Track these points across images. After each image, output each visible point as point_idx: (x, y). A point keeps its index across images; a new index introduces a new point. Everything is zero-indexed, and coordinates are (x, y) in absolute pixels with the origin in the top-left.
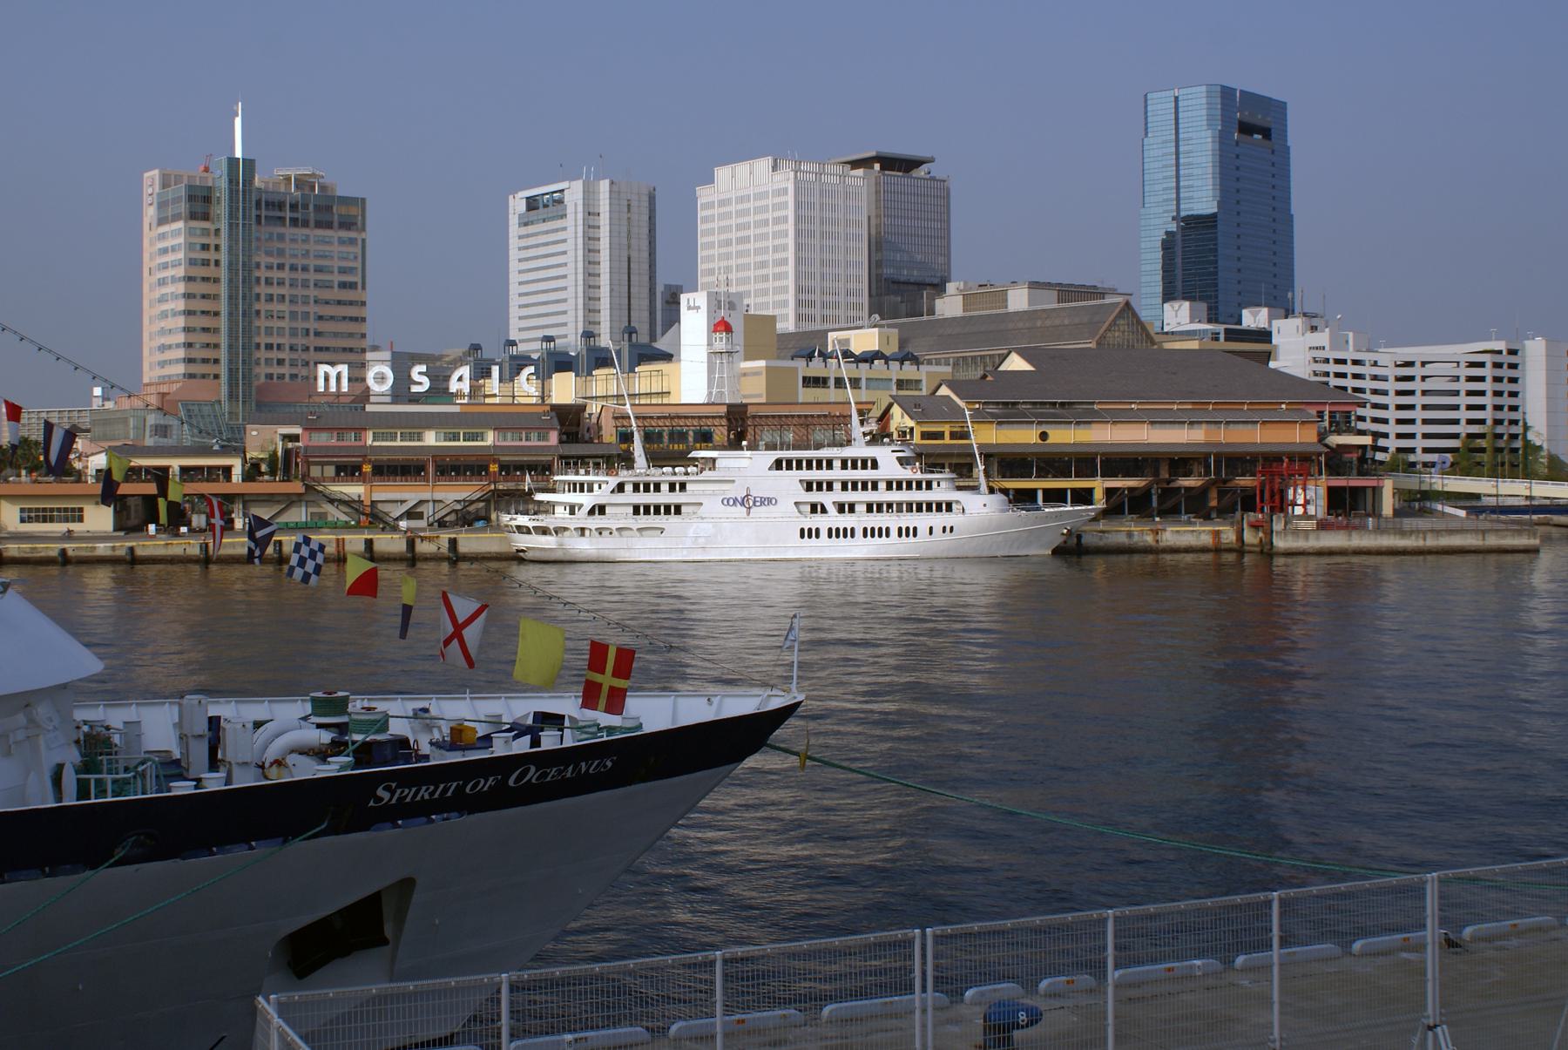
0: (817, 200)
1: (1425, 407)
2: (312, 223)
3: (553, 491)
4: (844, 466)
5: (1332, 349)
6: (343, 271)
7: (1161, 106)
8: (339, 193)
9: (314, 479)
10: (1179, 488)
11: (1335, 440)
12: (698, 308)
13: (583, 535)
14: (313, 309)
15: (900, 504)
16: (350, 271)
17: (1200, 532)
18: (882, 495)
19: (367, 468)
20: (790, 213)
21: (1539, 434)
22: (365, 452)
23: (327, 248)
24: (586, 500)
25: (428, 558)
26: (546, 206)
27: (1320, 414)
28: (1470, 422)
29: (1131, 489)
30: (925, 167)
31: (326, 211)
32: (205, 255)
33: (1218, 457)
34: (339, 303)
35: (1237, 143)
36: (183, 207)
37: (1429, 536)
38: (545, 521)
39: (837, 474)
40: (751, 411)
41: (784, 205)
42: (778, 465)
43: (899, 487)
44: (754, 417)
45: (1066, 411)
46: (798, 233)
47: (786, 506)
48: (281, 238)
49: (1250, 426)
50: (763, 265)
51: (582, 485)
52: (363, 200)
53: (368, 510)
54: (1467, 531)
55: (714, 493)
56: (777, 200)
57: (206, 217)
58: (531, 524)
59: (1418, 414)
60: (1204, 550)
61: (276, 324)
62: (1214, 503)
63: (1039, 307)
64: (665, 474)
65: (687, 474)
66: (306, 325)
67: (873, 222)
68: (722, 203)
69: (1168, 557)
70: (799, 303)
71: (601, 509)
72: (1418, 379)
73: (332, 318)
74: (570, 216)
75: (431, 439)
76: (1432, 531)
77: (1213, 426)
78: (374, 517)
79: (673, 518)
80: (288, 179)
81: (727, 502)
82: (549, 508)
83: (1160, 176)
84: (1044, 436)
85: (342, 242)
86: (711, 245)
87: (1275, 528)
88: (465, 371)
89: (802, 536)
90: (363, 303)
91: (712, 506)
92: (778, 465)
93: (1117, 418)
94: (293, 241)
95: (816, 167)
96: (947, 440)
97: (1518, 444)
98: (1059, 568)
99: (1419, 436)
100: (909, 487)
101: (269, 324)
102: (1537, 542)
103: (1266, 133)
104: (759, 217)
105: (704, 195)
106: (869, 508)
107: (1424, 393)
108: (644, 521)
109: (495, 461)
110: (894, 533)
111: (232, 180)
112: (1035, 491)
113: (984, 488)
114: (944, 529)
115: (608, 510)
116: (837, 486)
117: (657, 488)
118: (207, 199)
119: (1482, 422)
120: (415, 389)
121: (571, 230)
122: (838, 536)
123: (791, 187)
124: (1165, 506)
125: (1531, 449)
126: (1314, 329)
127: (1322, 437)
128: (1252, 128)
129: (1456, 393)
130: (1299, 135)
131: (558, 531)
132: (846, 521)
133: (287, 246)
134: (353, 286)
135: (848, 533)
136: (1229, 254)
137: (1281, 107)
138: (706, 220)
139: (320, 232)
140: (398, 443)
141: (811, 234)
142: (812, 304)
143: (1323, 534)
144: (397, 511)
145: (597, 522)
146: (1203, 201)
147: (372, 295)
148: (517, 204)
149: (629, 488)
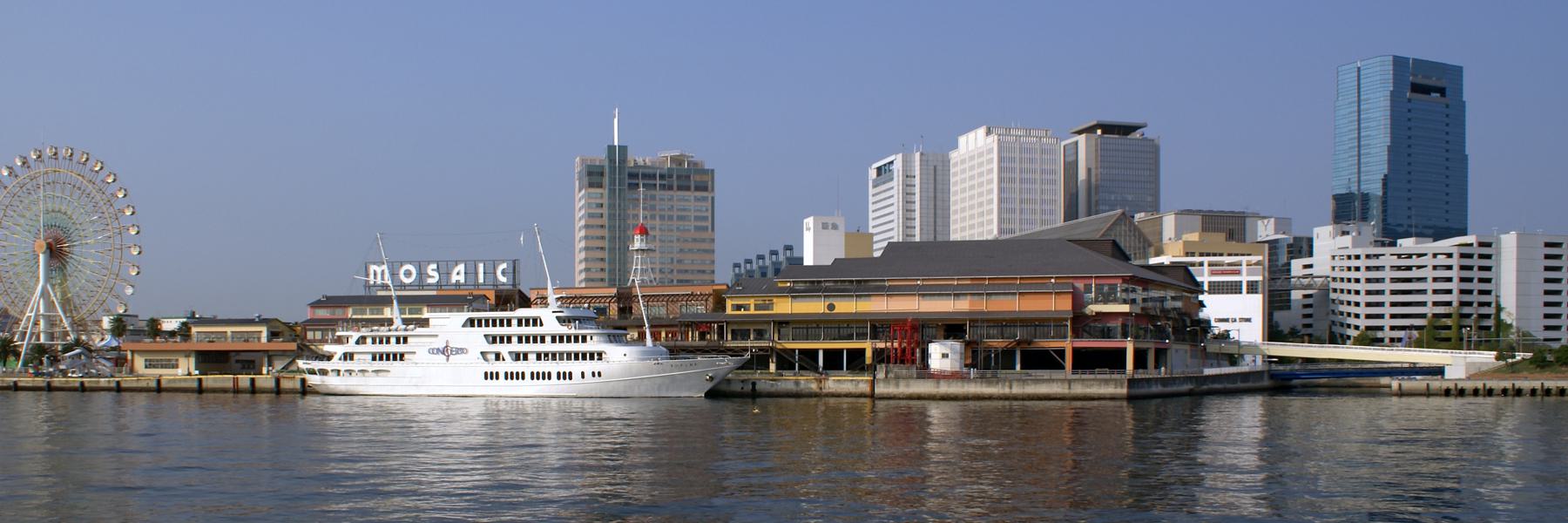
0: (1017, 155)
6: (697, 218)
15: (561, 354)
16: (705, 218)
18: (549, 347)
21: (1510, 314)
25: (264, 391)
31: (688, 178)
34: (695, 240)
36: (586, 180)
39: (515, 330)
43: (561, 340)
46: (1001, 180)
67: (1093, 172)
69: (832, 401)
79: (398, 363)
81: (432, 351)
84: (831, 307)
85: (697, 199)
88: (461, 267)
93: (892, 292)
96: (752, 311)
97: (1490, 322)
100: (569, 340)
103: (1442, 91)
108: (378, 365)
110: (554, 376)
112: (816, 351)
116: (515, 339)
119: (1449, 304)
120: (430, 281)
125: (1501, 325)
126: (1345, 233)
132: (519, 366)
137: (1458, 71)
141: (1012, 180)
145: (348, 365)
147: (718, 235)
149: (369, 340)
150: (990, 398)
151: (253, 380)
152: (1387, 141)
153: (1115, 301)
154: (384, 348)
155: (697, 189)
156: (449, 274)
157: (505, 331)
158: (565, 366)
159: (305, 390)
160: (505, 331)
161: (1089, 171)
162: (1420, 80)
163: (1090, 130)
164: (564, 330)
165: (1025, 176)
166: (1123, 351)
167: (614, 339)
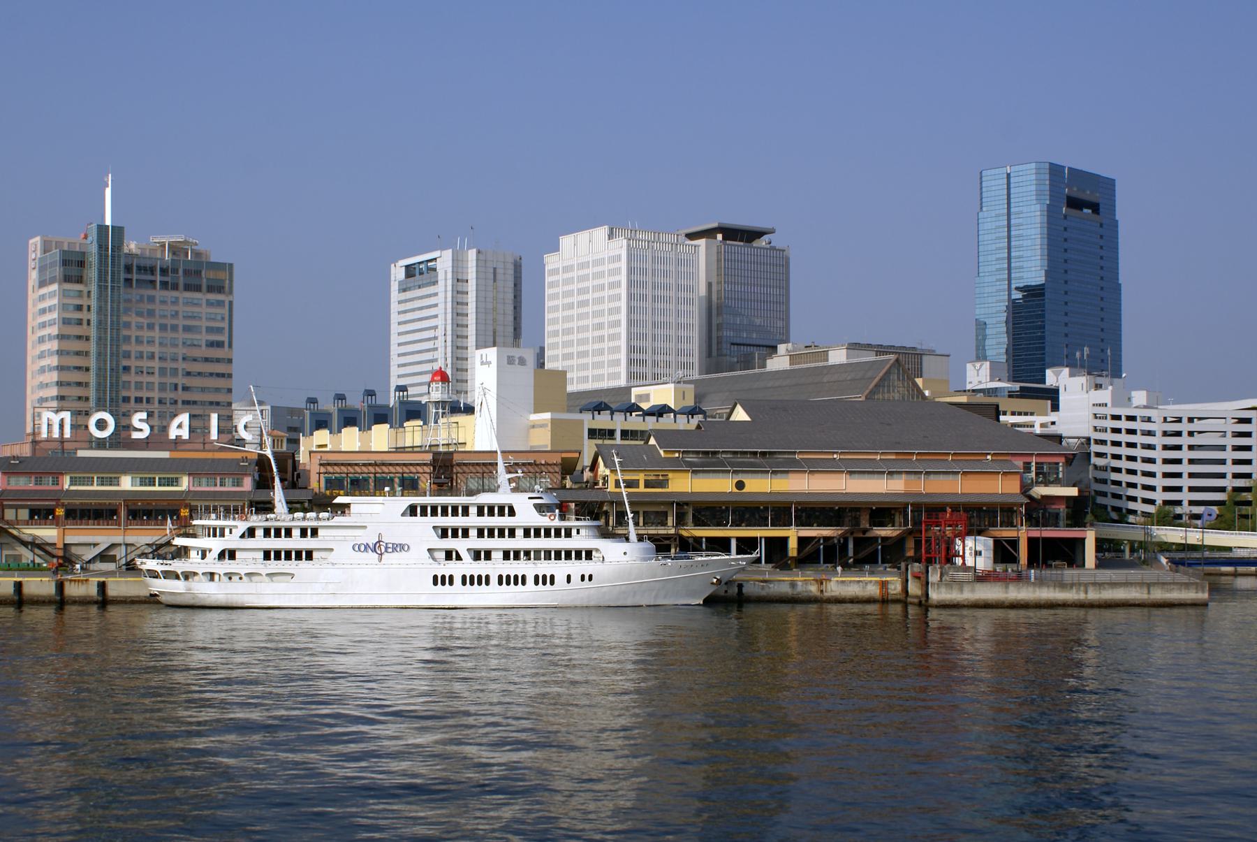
0: (649, 266)
1: (1191, 461)
2: (181, 286)
3: (194, 536)
4: (480, 512)
5: (1113, 406)
6: (210, 330)
7: (994, 183)
8: (213, 259)
9: (8, 523)
10: (876, 538)
11: (1040, 491)
12: (489, 363)
13: (212, 579)
14: (181, 365)
15: (537, 552)
16: (219, 330)
17: (867, 583)
18: (520, 543)
19: (60, 512)
20: (623, 278)
22: (58, 496)
23: (196, 309)
24: (216, 545)
25: (39, 602)
26: (421, 273)
27: (1027, 467)
28: (1236, 476)
29: (826, 539)
30: (766, 237)
31: (195, 275)
32: (78, 315)
33: (917, 507)
34: (207, 360)
35: (1065, 217)
36: (58, 271)
37: (1090, 589)
38: (178, 566)
39: (473, 520)
40: (457, 458)
41: (618, 271)
42: (412, 510)
43: (537, 534)
44: (459, 465)
45: (768, 461)
46: (630, 297)
47: (418, 553)
48: (151, 299)
49: (951, 477)
50: (599, 326)
51: (215, 529)
52: (231, 265)
53: (61, 553)
54: (1131, 584)
55: (345, 539)
56: (612, 266)
57: (80, 280)
58: (159, 568)
59: (1185, 468)
60: (870, 601)
61: (145, 379)
62: (910, 553)
63: (797, 367)
64: (300, 520)
65: (318, 519)
66: (174, 381)
67: (714, 288)
68: (567, 269)
70: (630, 362)
71: (232, 554)
72: (1185, 434)
73: (199, 374)
74: (441, 283)
75: (127, 483)
76: (1094, 584)
77: (913, 477)
78: (65, 560)
79: (304, 564)
80: (163, 246)
81: (357, 548)
82: (183, 552)
83: (994, 247)
84: (740, 485)
85: (210, 304)
86: (555, 309)
87: (931, 579)
88: (184, 418)
89: (435, 583)
90: (230, 361)
91: (343, 552)
92: (412, 510)
93: (814, 468)
94: (163, 302)
95: (650, 236)
96: (642, 489)
98: (708, 621)
99: (1185, 489)
100: (548, 534)
101: (139, 379)
102: (1206, 596)
103: (1095, 208)
104: (596, 282)
105: (551, 262)
106: (506, 555)
107: (1191, 448)
108: (273, 566)
109: (186, 507)
110: (530, 580)
111: (102, 246)
113: (633, 536)
114: (583, 578)
115: (238, 555)
116: (473, 533)
117: (289, 533)
118: (81, 264)
120: (135, 435)
121: (441, 295)
122: (508, 583)
123: (624, 254)
124: (861, 555)
126: (1098, 387)
127: (1025, 489)
128: (1081, 205)
129: (1222, 448)
130: (1128, 211)
131: (187, 576)
132: (481, 568)
133: (157, 307)
134: (219, 344)
135: (484, 580)
136: (1062, 321)
137: (1109, 184)
138: (552, 285)
139: (188, 295)
140: (95, 488)
141: (643, 298)
142: (643, 363)
143: (978, 586)
144: (90, 554)
145: (228, 566)
146: (1033, 272)
148: (398, 272)
149: (259, 533)
150: (1064, 605)
151: (18, 586)
153: (1057, 482)
154: (282, 543)
155: (210, 289)
156: (165, 429)
157: (459, 521)
158: (545, 567)
159: (103, 601)
160: (459, 521)
161: (709, 285)
162: (1076, 193)
163: (708, 234)
164: (544, 521)
165: (658, 292)
167: (605, 534)
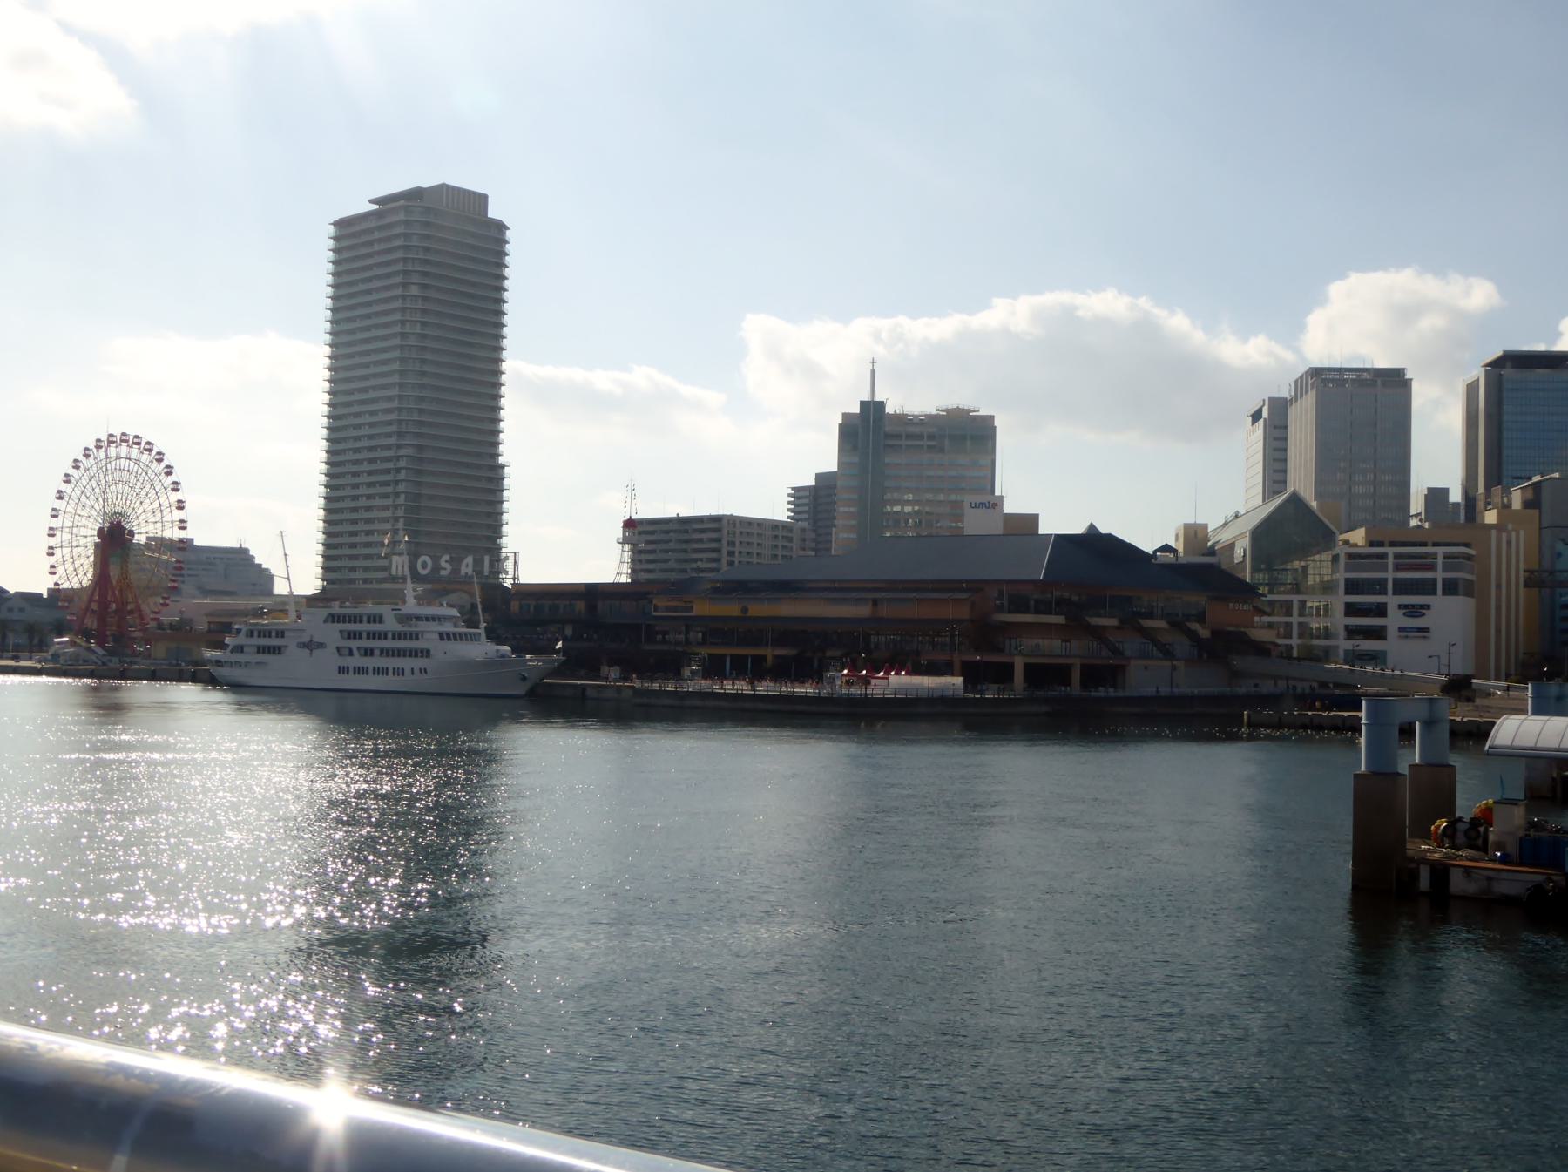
112: (724, 656)
152: (426, 185)
166: (1012, 666)
